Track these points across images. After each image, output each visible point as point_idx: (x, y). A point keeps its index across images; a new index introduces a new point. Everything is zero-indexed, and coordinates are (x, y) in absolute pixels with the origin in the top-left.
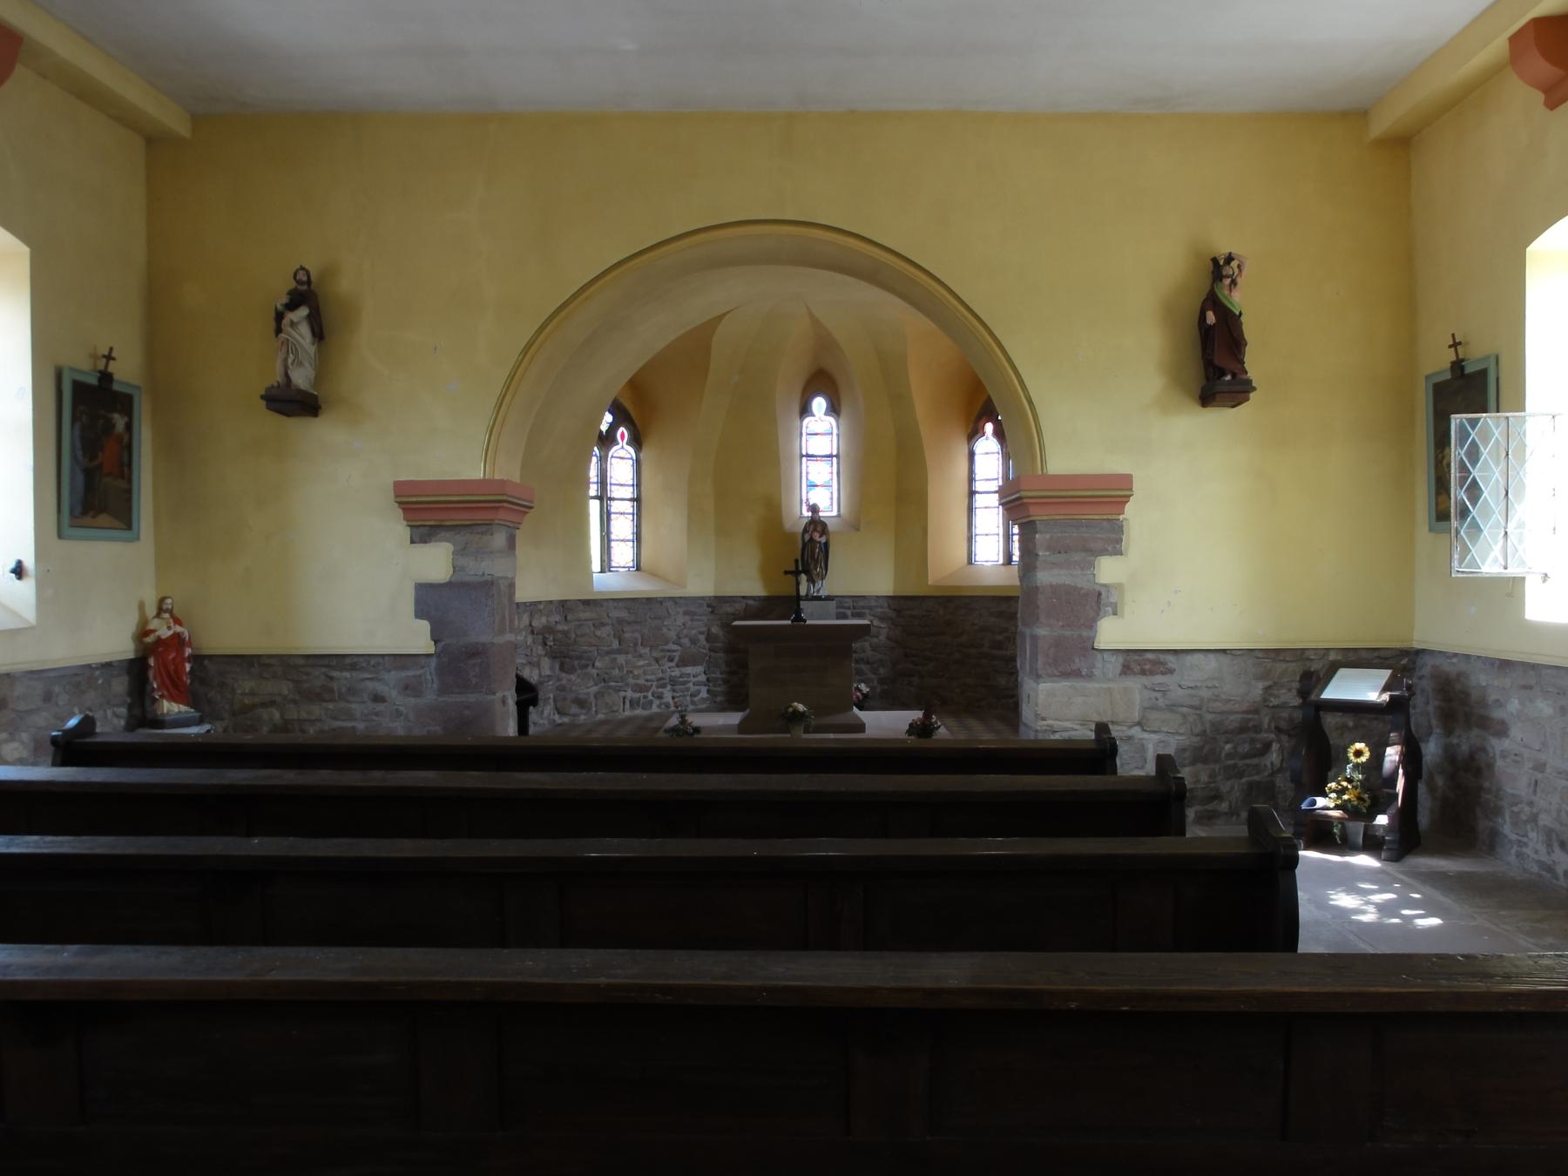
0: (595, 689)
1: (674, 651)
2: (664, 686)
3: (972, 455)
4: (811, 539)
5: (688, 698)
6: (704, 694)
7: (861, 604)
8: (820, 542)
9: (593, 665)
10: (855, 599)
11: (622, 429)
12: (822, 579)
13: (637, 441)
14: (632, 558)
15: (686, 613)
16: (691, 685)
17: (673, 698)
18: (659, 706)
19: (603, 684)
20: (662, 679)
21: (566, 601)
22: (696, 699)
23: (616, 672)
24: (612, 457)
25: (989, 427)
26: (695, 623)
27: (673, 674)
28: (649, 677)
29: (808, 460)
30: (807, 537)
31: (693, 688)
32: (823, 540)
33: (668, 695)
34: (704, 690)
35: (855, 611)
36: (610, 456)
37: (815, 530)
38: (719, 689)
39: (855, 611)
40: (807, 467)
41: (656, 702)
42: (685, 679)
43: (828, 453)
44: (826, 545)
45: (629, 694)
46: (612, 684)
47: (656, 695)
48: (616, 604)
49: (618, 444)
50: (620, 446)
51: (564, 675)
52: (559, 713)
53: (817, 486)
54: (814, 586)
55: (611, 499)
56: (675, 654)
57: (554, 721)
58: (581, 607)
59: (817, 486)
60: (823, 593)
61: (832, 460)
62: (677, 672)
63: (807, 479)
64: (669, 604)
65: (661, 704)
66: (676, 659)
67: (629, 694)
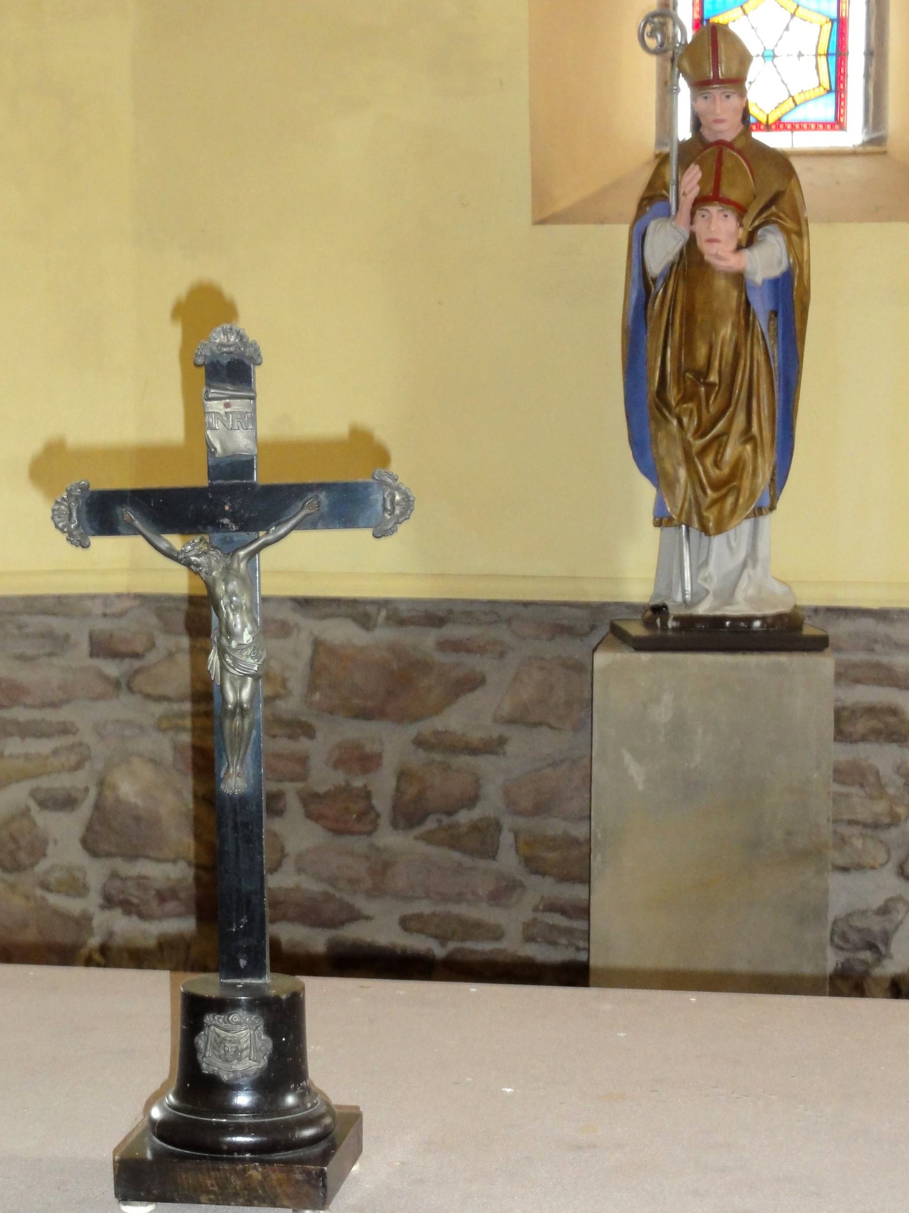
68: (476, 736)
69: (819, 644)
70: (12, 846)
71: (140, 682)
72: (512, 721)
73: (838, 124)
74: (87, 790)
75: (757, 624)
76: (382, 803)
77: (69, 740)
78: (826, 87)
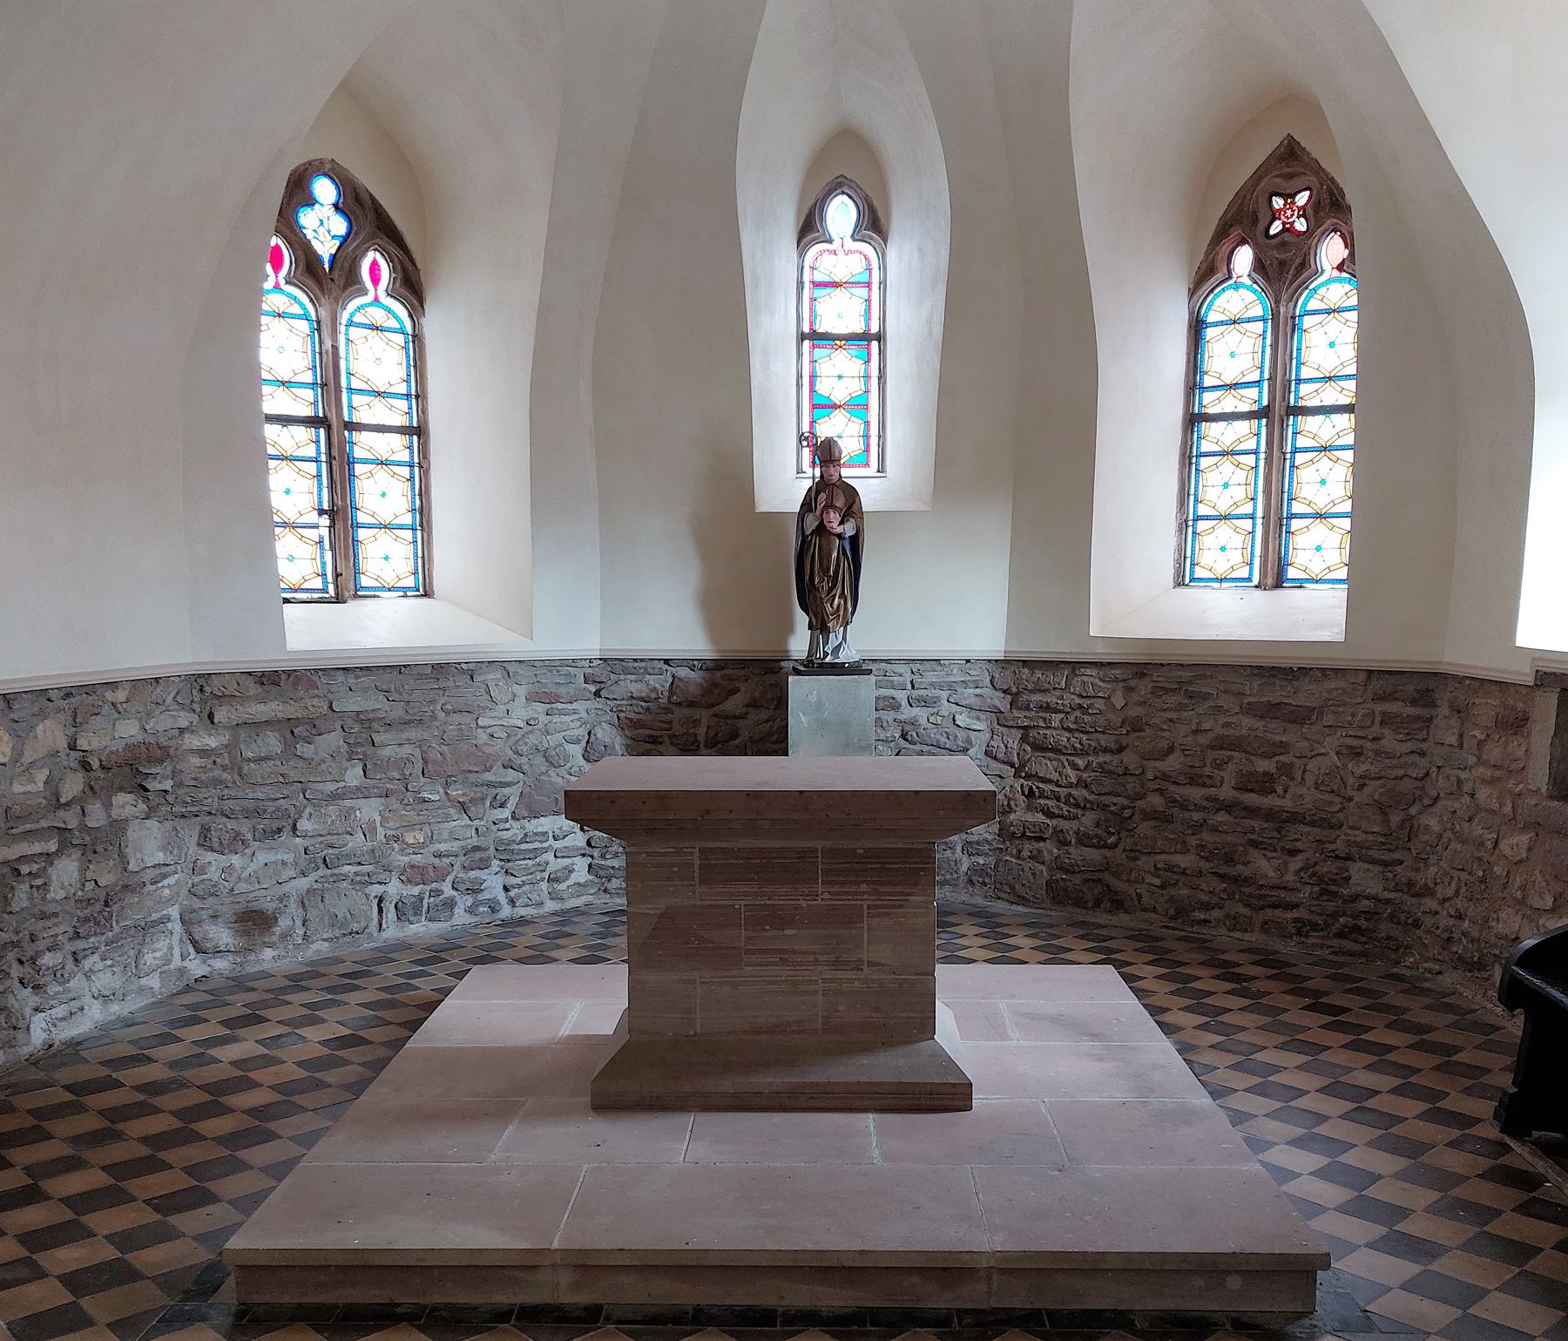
0: (303, 884)
1: (508, 784)
2: (483, 865)
3: (1197, 327)
4: (821, 529)
5: (544, 886)
6: (581, 874)
7: (931, 677)
8: (840, 536)
9: (294, 828)
10: (915, 667)
11: (371, 255)
12: (846, 624)
13: (411, 288)
14: (411, 568)
15: (532, 698)
16: (550, 856)
17: (506, 889)
18: (471, 911)
19: (323, 871)
20: (477, 849)
21: (208, 676)
22: (563, 886)
23: (357, 841)
24: (350, 324)
25: (1244, 258)
26: (556, 719)
27: (505, 835)
28: (443, 847)
29: (814, 347)
30: (811, 523)
31: (555, 865)
32: (849, 529)
33: (493, 883)
34: (581, 864)
35: (916, 693)
36: (344, 321)
37: (830, 506)
38: (616, 863)
39: (916, 693)
40: (813, 362)
41: (464, 902)
42: (537, 845)
43: (859, 328)
44: (856, 541)
45: (394, 889)
46: (347, 868)
47: (462, 887)
48: (351, 681)
49: (364, 292)
50: (370, 297)
51: (210, 857)
52: (199, 950)
53: (835, 407)
54: (826, 642)
55: (352, 426)
56: (506, 791)
57: (182, 971)
58: (253, 689)
59: (835, 407)
60: (847, 656)
61: (868, 347)
62: (515, 830)
63: (812, 390)
64: (493, 676)
65: (476, 904)
66: (511, 804)
67: (394, 889)
68: (738, 712)
69: (869, 672)
70: (557, 758)
71: (603, 693)
72: (748, 706)
73: (867, 465)
74: (584, 736)
75: (847, 665)
76: (701, 739)
77: (577, 716)
78: (1370, 1238)
